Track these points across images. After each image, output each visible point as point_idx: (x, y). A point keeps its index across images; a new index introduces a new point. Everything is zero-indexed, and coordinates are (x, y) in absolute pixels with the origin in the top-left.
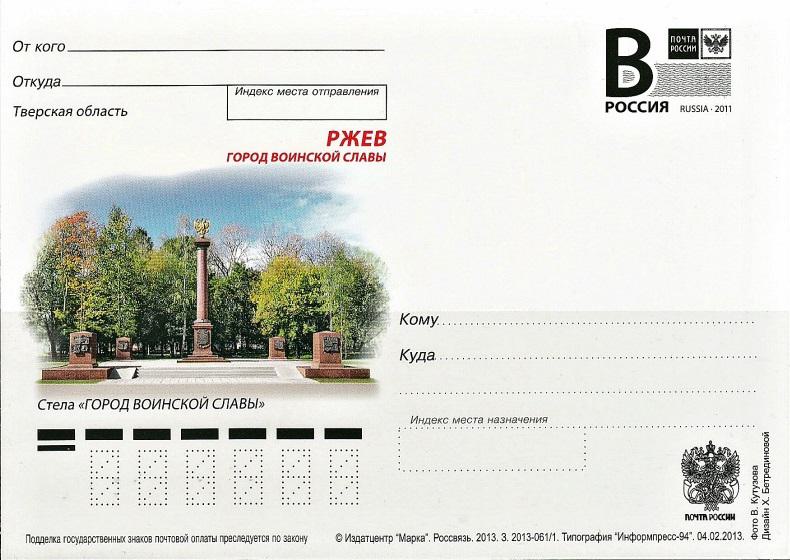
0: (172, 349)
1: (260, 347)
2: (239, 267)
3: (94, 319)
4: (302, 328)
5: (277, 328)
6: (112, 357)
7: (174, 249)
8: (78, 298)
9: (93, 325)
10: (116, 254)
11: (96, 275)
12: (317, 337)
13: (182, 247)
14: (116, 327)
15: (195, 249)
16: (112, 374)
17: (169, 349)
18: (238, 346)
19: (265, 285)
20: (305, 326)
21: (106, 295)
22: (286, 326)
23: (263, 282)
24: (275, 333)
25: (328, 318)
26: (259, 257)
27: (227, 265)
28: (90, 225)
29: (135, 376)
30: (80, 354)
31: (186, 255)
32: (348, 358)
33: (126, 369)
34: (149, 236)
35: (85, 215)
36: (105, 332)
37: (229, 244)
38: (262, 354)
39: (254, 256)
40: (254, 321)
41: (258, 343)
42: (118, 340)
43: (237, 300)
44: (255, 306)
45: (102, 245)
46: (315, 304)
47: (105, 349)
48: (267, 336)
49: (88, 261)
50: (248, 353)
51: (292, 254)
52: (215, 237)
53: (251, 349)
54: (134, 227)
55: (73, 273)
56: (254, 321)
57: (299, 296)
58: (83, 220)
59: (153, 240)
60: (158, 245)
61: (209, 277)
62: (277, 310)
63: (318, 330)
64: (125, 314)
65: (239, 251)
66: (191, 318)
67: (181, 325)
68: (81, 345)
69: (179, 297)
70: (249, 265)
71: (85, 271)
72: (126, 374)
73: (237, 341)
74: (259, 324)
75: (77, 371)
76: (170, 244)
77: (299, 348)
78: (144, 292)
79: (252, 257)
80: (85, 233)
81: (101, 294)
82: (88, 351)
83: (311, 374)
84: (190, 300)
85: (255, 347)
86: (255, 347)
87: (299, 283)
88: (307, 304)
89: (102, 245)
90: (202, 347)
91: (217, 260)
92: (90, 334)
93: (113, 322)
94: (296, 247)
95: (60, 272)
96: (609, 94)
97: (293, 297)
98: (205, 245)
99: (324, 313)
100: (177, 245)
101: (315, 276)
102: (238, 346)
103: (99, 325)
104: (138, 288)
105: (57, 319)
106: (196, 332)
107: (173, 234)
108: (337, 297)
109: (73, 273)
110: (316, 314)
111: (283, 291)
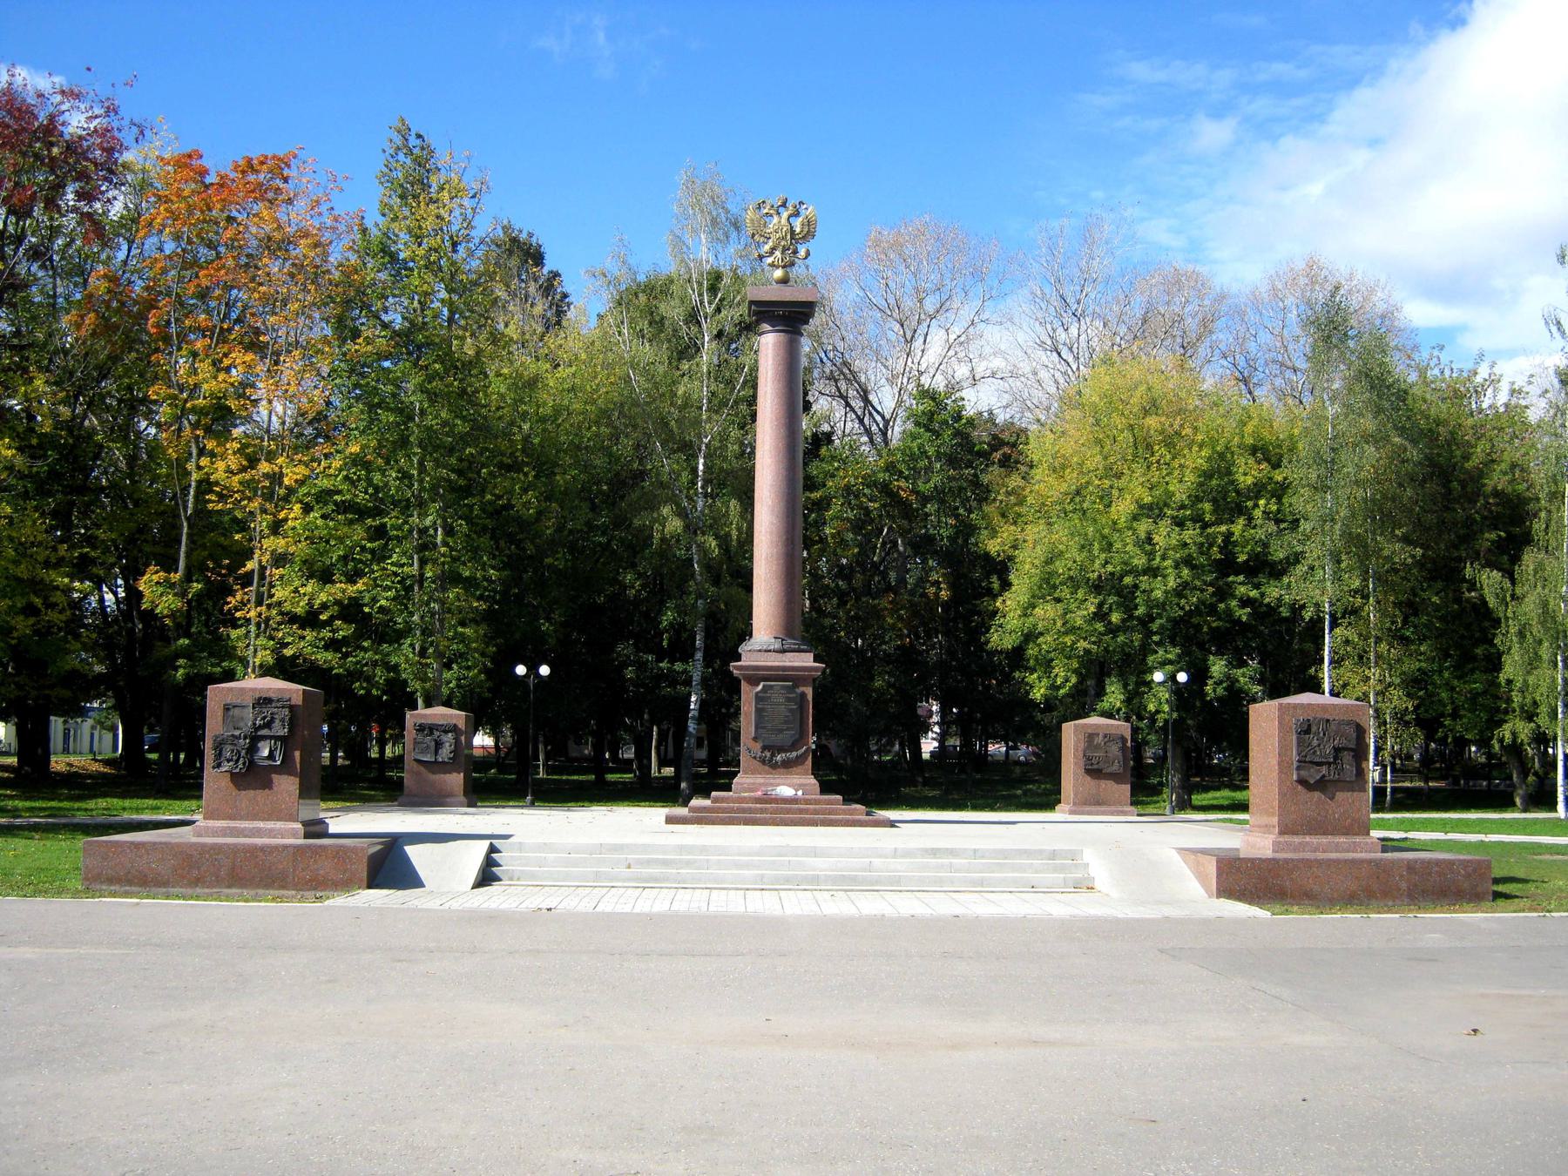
0: (642, 754)
1: (1023, 752)
2: (936, 413)
3: (310, 620)
4: (1200, 675)
5: (1094, 672)
6: (382, 785)
7: (658, 323)
8: (242, 525)
9: (304, 644)
10: (409, 341)
11: (317, 428)
12: (1267, 722)
13: (693, 317)
14: (405, 655)
15: (748, 328)
16: (388, 866)
17: (629, 753)
18: (928, 745)
19: (1045, 486)
20: (1218, 667)
21: (361, 513)
22: (1133, 667)
23: (1038, 473)
24: (1082, 701)
25: (1314, 632)
26: (1026, 368)
27: (885, 399)
28: (296, 216)
29: (487, 876)
30: (251, 776)
31: (709, 353)
32: (1397, 806)
33: (450, 841)
34: (550, 264)
35: (280, 166)
36: (356, 675)
37: (894, 310)
38: (1032, 787)
39: (1000, 362)
40: (1001, 638)
41: (1012, 736)
42: (411, 717)
43: (923, 546)
44: (1000, 569)
45: (349, 306)
46: (1263, 567)
47: (357, 751)
48: (1049, 704)
49: (290, 366)
50: (967, 783)
51: (1165, 358)
52: (837, 276)
53: (983, 759)
54: (484, 227)
55: (219, 418)
56: (1001, 638)
57: (1191, 534)
58: (267, 194)
59: (568, 284)
60: (589, 305)
61: (809, 450)
62: (1097, 588)
63: (1276, 690)
64: (423, 577)
65: (937, 339)
66: (731, 626)
67: (681, 650)
68: (255, 740)
69: (675, 525)
70: (978, 400)
71: (273, 411)
72: (445, 870)
73: (926, 728)
74: (1017, 656)
75: (235, 849)
76: (644, 302)
77: (1189, 761)
78: (527, 503)
79: (998, 363)
80: (277, 245)
81: (343, 508)
82: (286, 767)
83: (1240, 879)
84: (724, 541)
85: (996, 749)
86: (996, 749)
87: (1190, 478)
88: (1227, 565)
89: (349, 306)
90: (775, 758)
91: (844, 377)
92: (293, 690)
93: (387, 634)
94: (1175, 319)
95: (164, 412)
96: (1048, 800)
97: (1165, 535)
98: (792, 317)
99: (1297, 609)
100: (672, 311)
101: (1260, 451)
102: (928, 745)
103: (333, 645)
104: (502, 483)
105: (149, 616)
106: (748, 694)
107: (654, 258)
108: (1351, 539)
109: (219, 418)
110: (1264, 613)
111: (1122, 508)
